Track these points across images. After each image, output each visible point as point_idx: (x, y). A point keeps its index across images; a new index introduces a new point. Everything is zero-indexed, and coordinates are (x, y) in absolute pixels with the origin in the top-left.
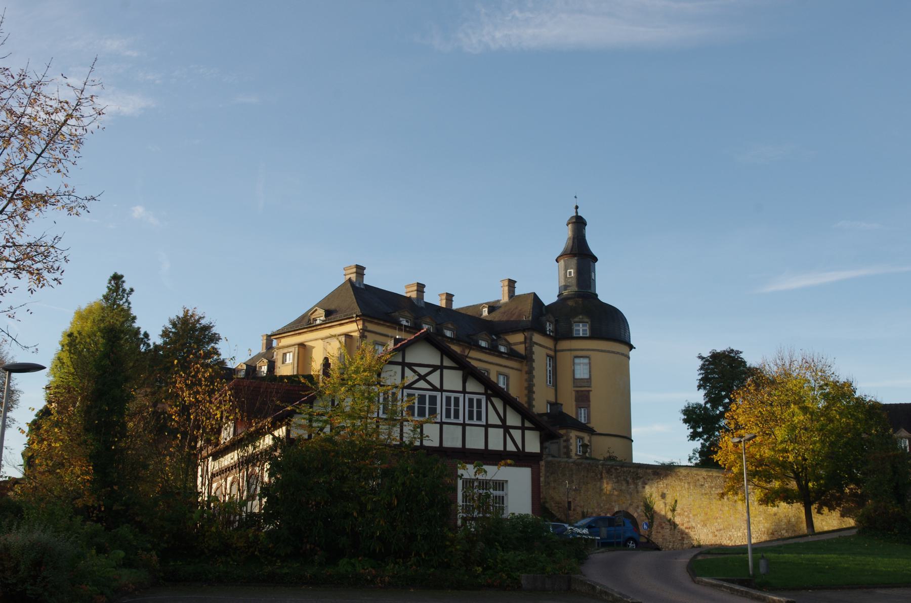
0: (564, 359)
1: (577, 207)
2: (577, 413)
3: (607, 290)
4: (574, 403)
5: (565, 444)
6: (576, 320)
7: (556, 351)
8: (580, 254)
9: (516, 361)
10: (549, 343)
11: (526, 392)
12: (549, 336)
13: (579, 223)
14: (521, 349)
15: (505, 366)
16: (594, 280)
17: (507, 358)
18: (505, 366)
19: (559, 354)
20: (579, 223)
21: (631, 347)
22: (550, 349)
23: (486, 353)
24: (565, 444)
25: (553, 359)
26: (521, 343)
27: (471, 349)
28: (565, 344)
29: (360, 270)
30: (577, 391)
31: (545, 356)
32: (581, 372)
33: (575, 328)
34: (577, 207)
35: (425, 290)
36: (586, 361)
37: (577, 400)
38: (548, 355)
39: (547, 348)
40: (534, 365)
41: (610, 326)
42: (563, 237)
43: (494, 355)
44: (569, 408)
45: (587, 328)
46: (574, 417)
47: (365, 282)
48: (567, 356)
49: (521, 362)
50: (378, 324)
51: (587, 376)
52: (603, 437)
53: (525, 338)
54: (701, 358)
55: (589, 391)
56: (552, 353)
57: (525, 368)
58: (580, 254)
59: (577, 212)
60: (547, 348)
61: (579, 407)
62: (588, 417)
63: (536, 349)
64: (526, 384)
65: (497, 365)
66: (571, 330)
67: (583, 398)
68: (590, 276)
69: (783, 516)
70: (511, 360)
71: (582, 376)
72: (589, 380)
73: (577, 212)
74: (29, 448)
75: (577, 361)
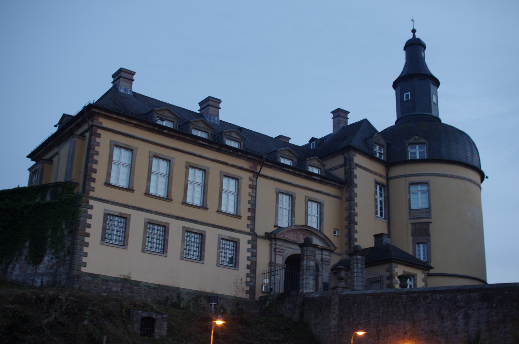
0: (399, 186)
1: (414, 31)
2: (414, 250)
3: (450, 109)
4: (410, 239)
5: (389, 282)
6: (411, 140)
7: (388, 179)
8: (416, 82)
9: (332, 185)
10: (379, 169)
11: (346, 223)
12: (378, 160)
13: (415, 48)
14: (340, 173)
16: (436, 104)
17: (320, 182)
19: (392, 182)
20: (415, 48)
21: (482, 176)
22: (380, 176)
23: (289, 173)
24: (389, 282)
25: (385, 187)
26: (341, 166)
27: (263, 165)
29: (123, 76)
31: (373, 183)
32: (419, 201)
33: (410, 150)
34: (414, 31)
35: (221, 105)
36: (424, 188)
38: (377, 183)
39: (376, 174)
40: (356, 190)
41: (454, 150)
43: (300, 176)
44: (404, 242)
45: (424, 150)
46: (411, 253)
47: (134, 89)
48: (402, 183)
49: (340, 188)
50: (120, 121)
51: (425, 206)
52: (447, 278)
53: (345, 159)
55: (428, 223)
56: (383, 181)
57: (346, 195)
58: (416, 82)
59: (414, 36)
60: (376, 174)
61: (417, 243)
62: (428, 253)
63: (357, 172)
64: (346, 214)
67: (421, 231)
68: (430, 99)
70: (326, 184)
71: (421, 206)
72: (428, 210)
73: (414, 36)
74: (223, 297)
75: (413, 189)
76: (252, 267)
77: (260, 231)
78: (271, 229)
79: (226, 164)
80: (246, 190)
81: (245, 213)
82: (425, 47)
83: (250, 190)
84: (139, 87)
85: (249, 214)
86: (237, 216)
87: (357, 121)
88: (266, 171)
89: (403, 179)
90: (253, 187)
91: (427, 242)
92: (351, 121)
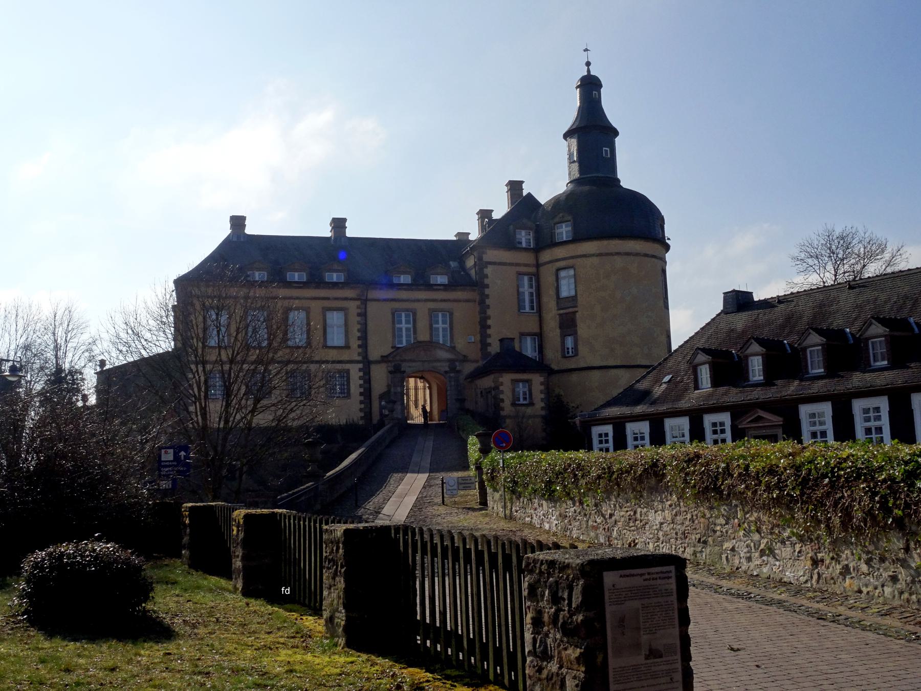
0: (547, 275)
1: (588, 64)
3: (631, 175)
6: (557, 220)
8: (593, 133)
13: (590, 87)
15: (444, 301)
18: (444, 301)
19: (543, 270)
20: (590, 87)
22: (526, 265)
28: (546, 256)
29: (238, 222)
30: (560, 315)
34: (588, 64)
37: (561, 327)
41: (638, 222)
42: (569, 109)
51: (573, 293)
54: (339, 224)
58: (593, 133)
59: (589, 71)
65: (426, 300)
66: (552, 235)
67: (568, 325)
69: (446, 529)
72: (574, 299)
73: (589, 71)
76: (367, 393)
77: (375, 353)
78: (386, 350)
79: (328, 299)
80: (354, 320)
81: (355, 343)
82: (601, 86)
83: (359, 319)
84: (251, 229)
85: (360, 342)
86: (347, 347)
87: (665, 226)
88: (374, 294)
89: (550, 265)
90: (363, 315)
91: (574, 334)
92: (107, 367)
